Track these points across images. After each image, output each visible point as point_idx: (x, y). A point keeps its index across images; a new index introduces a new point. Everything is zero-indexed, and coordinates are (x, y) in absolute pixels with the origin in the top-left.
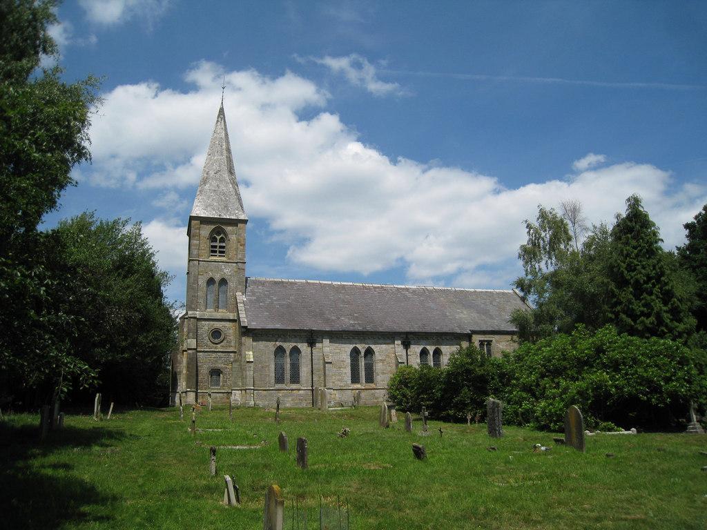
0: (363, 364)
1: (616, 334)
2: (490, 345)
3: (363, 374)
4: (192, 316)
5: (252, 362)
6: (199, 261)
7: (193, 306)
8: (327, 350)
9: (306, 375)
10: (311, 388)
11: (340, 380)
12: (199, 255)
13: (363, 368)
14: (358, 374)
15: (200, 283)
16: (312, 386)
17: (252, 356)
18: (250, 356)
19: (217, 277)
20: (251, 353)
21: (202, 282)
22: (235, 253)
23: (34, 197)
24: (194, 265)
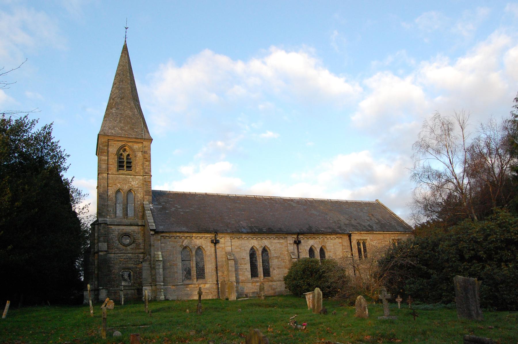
3: (260, 270)
5: (161, 261)
15: (109, 194)
17: (161, 256)
20: (160, 253)
22: (141, 168)
23: (444, 221)
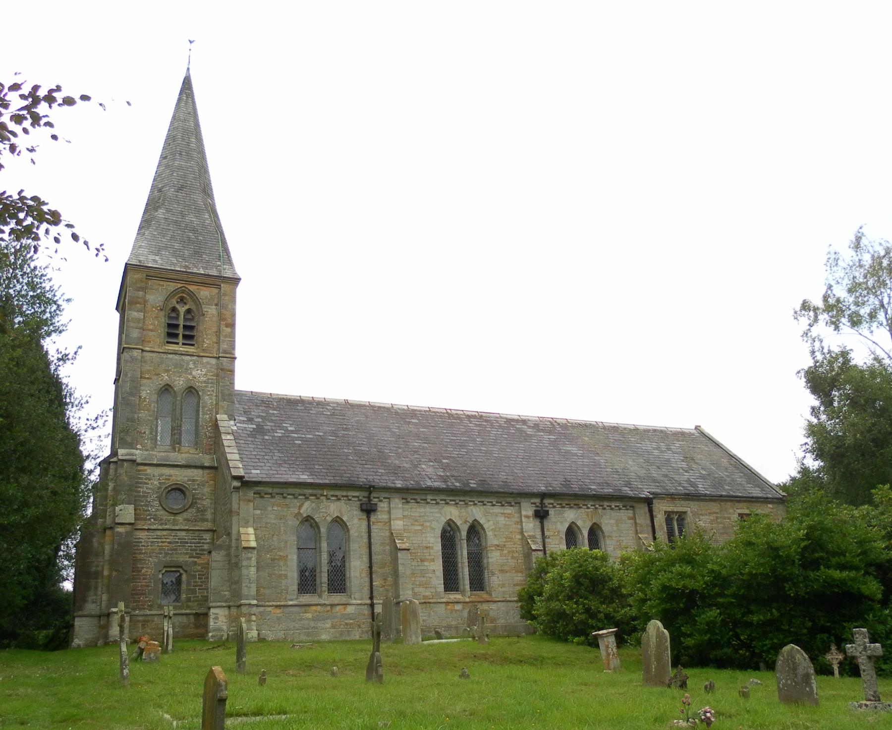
0: (465, 552)
1: (9, 357)
2: (683, 519)
3: (464, 572)
4: (124, 458)
5: (254, 548)
6: (143, 351)
7: (129, 439)
8: (398, 525)
9: (358, 574)
10: (369, 602)
11: (426, 585)
12: (143, 341)
13: (466, 560)
14: (455, 565)
15: (143, 394)
16: (371, 598)
17: (252, 537)
18: (249, 536)
19: (180, 383)
20: (251, 530)
21: (147, 391)
24: (133, 359)
